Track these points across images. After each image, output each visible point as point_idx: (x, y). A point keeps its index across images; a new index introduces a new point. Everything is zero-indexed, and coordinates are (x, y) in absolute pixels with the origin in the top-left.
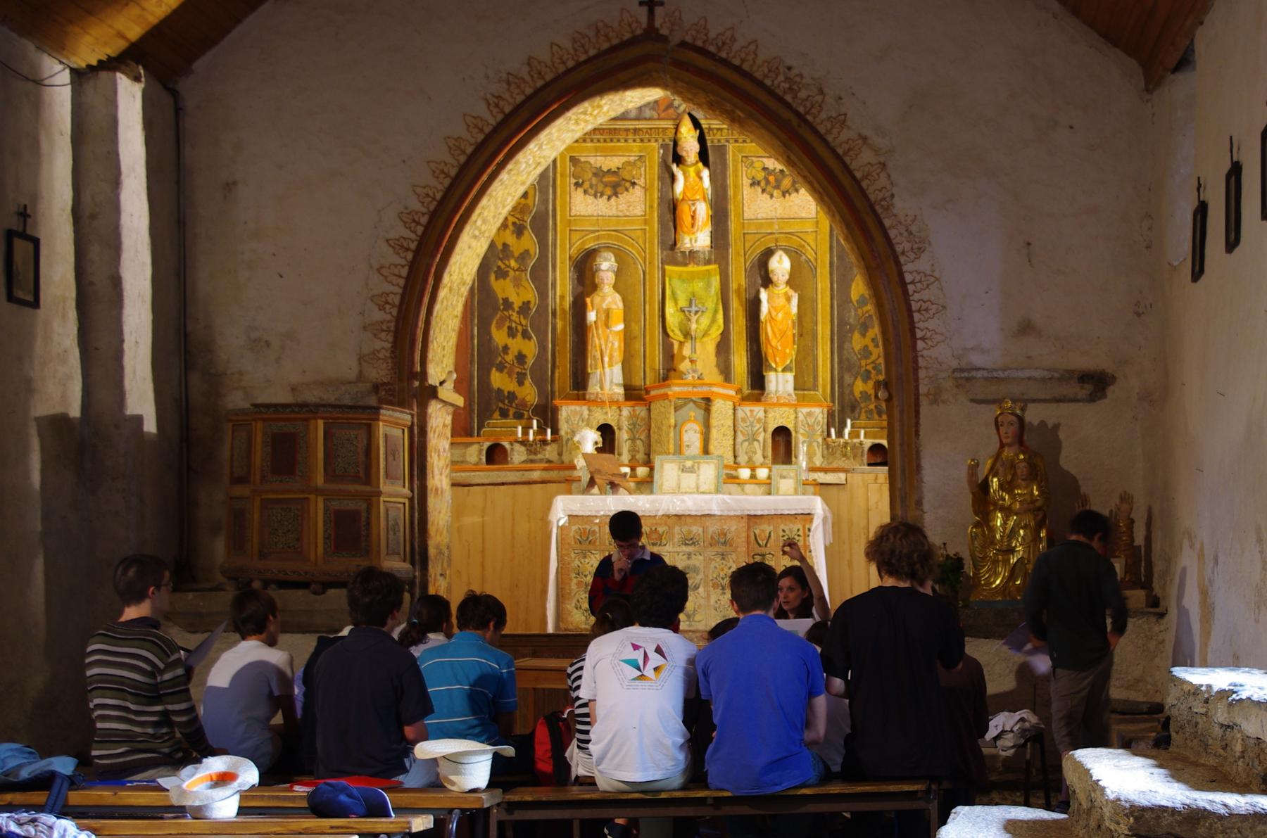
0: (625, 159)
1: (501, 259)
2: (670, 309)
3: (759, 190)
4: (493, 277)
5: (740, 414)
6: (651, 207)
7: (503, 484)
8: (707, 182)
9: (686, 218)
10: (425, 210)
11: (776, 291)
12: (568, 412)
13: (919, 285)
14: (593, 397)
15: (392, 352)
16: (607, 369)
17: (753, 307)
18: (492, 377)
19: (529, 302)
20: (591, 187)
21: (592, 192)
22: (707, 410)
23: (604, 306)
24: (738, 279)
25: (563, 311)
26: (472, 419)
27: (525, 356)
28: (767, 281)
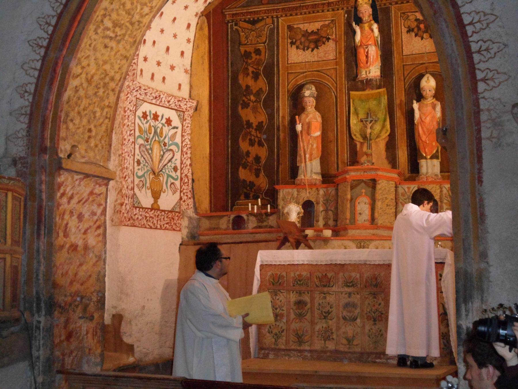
0: (321, 23)
1: (245, 96)
2: (353, 121)
3: (413, 34)
4: (240, 107)
5: (400, 190)
6: (340, 53)
7: (241, 243)
8: (376, 32)
9: (362, 57)
10: (54, 13)
11: (425, 102)
12: (283, 192)
13: (478, 26)
14: (298, 182)
15: (28, 131)
16: (308, 163)
17: (411, 113)
18: (240, 173)
19: (262, 122)
20: (301, 44)
21: (302, 47)
22: (374, 188)
23: (307, 120)
24: (400, 96)
25: (284, 126)
26: (228, 200)
27: (260, 158)
28: (420, 98)
